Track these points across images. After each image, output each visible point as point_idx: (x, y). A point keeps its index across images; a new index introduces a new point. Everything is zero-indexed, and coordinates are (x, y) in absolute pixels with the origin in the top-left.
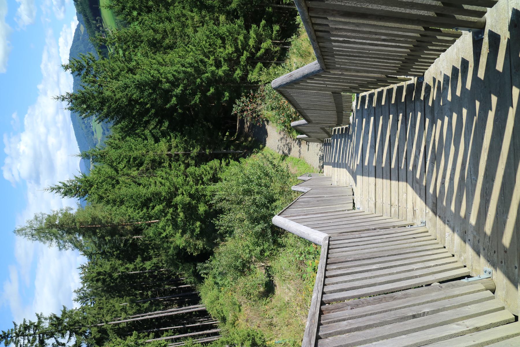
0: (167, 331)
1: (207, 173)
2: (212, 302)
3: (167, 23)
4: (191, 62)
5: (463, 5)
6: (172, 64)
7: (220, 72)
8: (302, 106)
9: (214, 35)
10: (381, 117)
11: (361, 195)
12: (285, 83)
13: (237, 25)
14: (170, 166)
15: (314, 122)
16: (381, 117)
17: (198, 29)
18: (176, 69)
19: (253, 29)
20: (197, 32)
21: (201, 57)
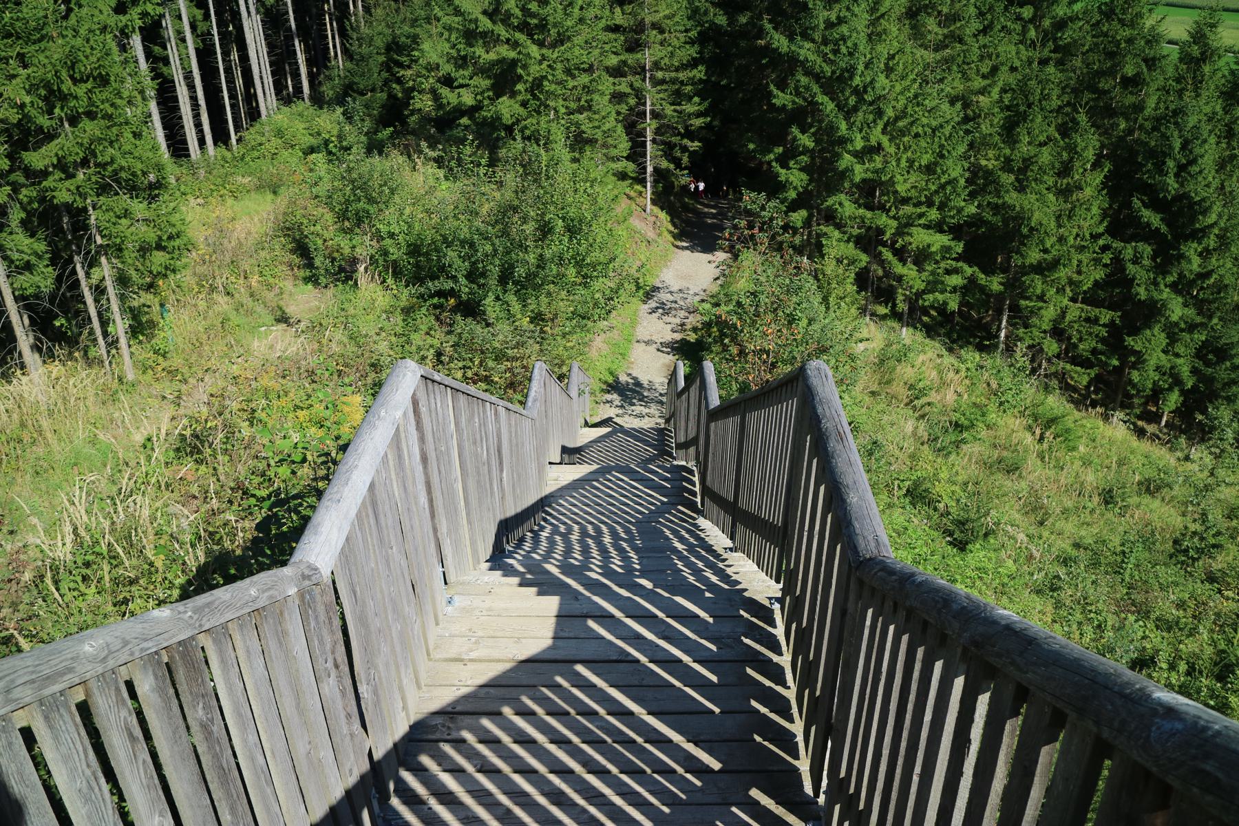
0: (207, 16)
1: (597, 124)
2: (279, 133)
3: (976, 25)
4: (877, 85)
5: (988, 695)
6: (874, 37)
7: (846, 160)
8: (753, 417)
9: (941, 146)
10: (714, 679)
11: (490, 609)
12: (820, 411)
13: (963, 204)
14: (616, 29)
15: (713, 424)
16: (714, 679)
17: (959, 105)
18: (861, 48)
19: (953, 244)
20: (952, 103)
21: (890, 113)
